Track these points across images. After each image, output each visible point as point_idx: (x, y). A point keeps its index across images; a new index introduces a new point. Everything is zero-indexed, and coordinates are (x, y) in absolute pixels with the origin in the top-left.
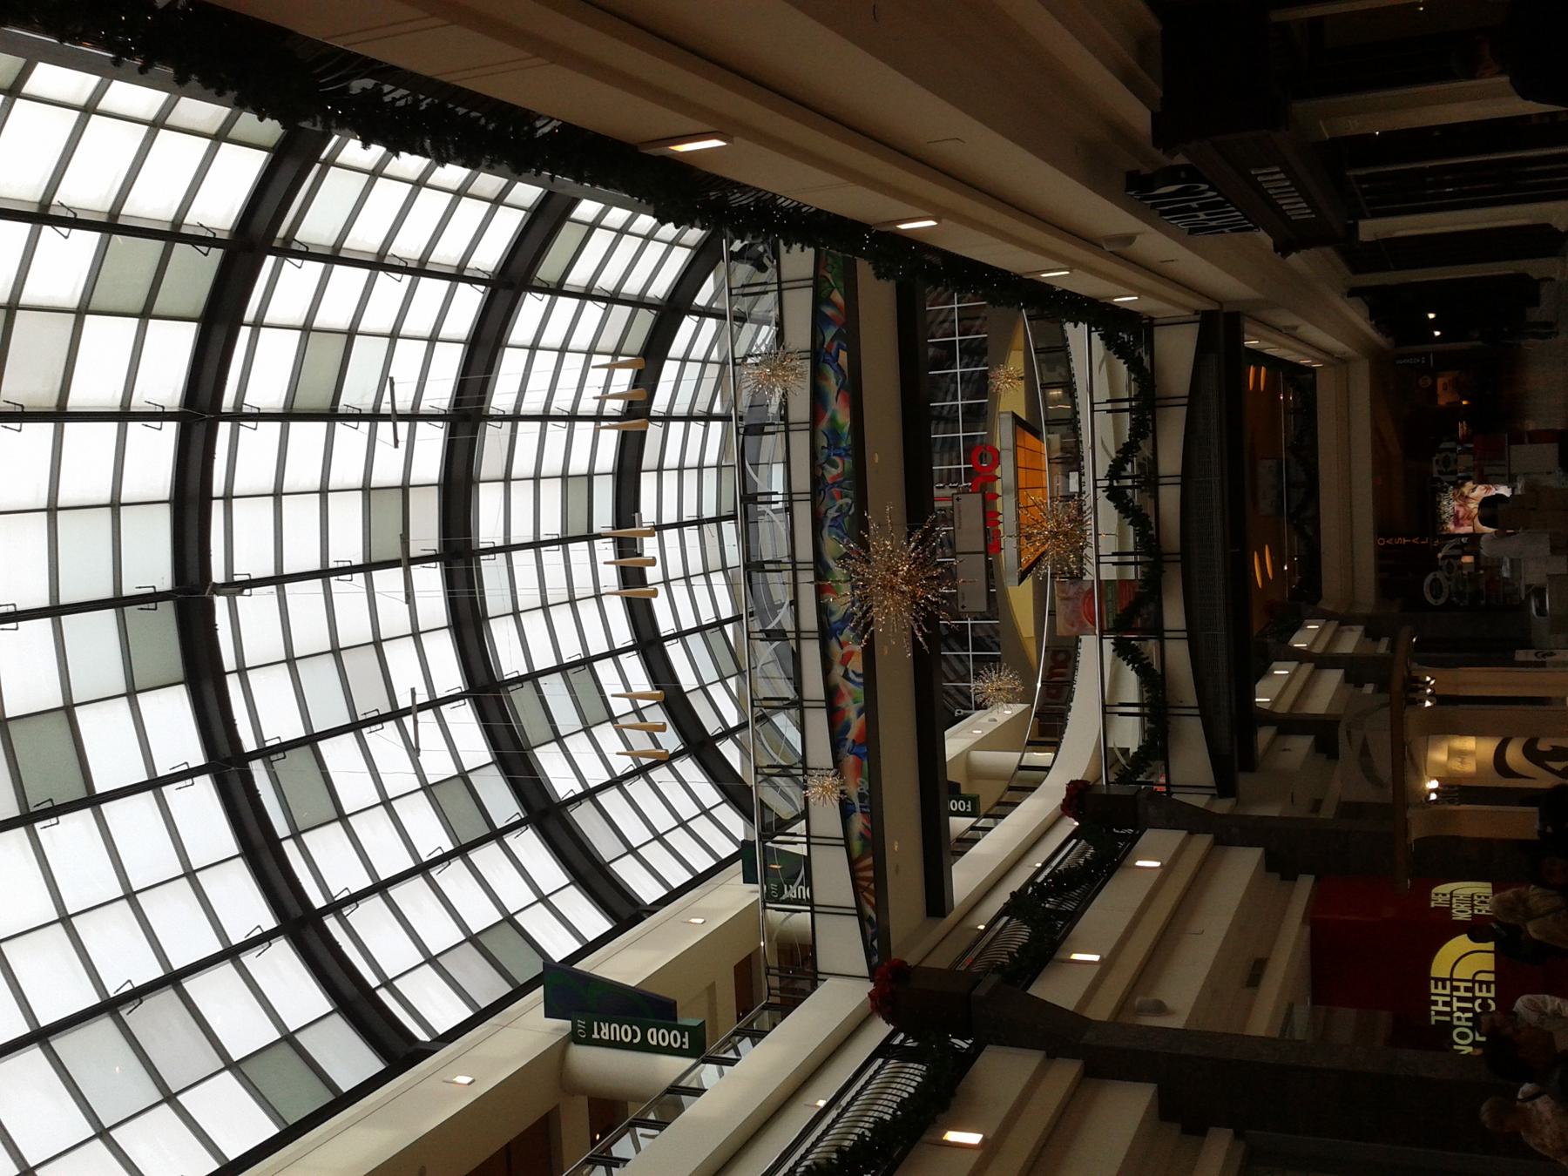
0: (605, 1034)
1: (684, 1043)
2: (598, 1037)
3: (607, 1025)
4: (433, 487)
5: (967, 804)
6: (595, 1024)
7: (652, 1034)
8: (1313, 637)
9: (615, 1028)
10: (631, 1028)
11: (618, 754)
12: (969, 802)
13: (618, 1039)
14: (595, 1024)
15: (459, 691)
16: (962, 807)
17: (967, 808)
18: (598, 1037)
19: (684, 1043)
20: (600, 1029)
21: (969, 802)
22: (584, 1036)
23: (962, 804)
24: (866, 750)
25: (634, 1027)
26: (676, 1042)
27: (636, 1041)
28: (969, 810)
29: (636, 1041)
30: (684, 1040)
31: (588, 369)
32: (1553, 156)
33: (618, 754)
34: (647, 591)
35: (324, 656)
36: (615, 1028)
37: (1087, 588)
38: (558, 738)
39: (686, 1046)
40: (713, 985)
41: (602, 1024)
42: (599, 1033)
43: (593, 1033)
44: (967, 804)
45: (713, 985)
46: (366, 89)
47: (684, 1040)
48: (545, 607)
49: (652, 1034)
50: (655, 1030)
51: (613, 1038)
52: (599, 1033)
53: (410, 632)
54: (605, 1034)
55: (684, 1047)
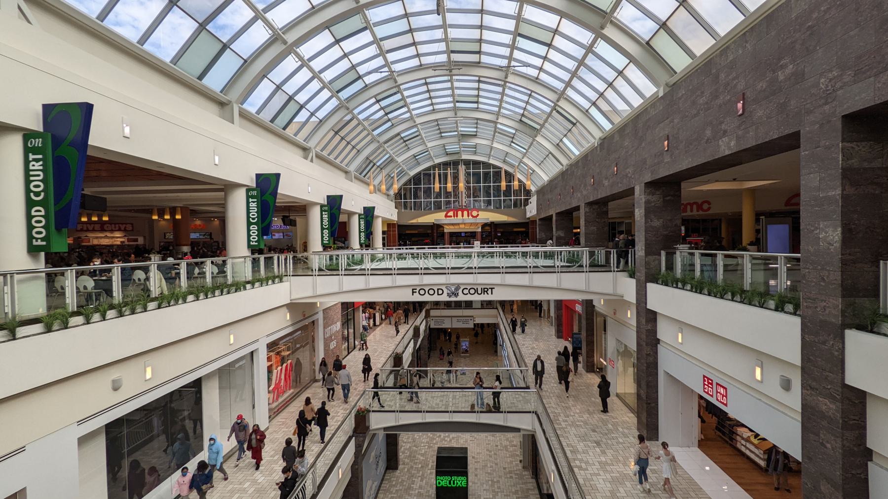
0: (33, 165)
1: (37, 241)
2: (30, 159)
3: (41, 168)
4: (333, 38)
5: (256, 242)
7: (40, 211)
8: (300, 126)
9: (39, 175)
10: (42, 191)
11: (22, 449)
12: (257, 244)
16: (253, 238)
17: (253, 242)
18: (30, 159)
19: (37, 241)
22: (29, 145)
25: (43, 194)
27: (32, 194)
29: (32, 194)
30: (39, 240)
31: (142, 50)
32: (447, 471)
33: (22, 449)
34: (282, 37)
35: (280, 309)
36: (39, 175)
38: (337, 42)
39: (251, 243)
41: (41, 163)
42: (252, 202)
43: (33, 154)
44: (256, 242)
47: (39, 240)
48: (620, 73)
49: (40, 211)
52: (252, 202)
54: (33, 165)
55: (34, 240)
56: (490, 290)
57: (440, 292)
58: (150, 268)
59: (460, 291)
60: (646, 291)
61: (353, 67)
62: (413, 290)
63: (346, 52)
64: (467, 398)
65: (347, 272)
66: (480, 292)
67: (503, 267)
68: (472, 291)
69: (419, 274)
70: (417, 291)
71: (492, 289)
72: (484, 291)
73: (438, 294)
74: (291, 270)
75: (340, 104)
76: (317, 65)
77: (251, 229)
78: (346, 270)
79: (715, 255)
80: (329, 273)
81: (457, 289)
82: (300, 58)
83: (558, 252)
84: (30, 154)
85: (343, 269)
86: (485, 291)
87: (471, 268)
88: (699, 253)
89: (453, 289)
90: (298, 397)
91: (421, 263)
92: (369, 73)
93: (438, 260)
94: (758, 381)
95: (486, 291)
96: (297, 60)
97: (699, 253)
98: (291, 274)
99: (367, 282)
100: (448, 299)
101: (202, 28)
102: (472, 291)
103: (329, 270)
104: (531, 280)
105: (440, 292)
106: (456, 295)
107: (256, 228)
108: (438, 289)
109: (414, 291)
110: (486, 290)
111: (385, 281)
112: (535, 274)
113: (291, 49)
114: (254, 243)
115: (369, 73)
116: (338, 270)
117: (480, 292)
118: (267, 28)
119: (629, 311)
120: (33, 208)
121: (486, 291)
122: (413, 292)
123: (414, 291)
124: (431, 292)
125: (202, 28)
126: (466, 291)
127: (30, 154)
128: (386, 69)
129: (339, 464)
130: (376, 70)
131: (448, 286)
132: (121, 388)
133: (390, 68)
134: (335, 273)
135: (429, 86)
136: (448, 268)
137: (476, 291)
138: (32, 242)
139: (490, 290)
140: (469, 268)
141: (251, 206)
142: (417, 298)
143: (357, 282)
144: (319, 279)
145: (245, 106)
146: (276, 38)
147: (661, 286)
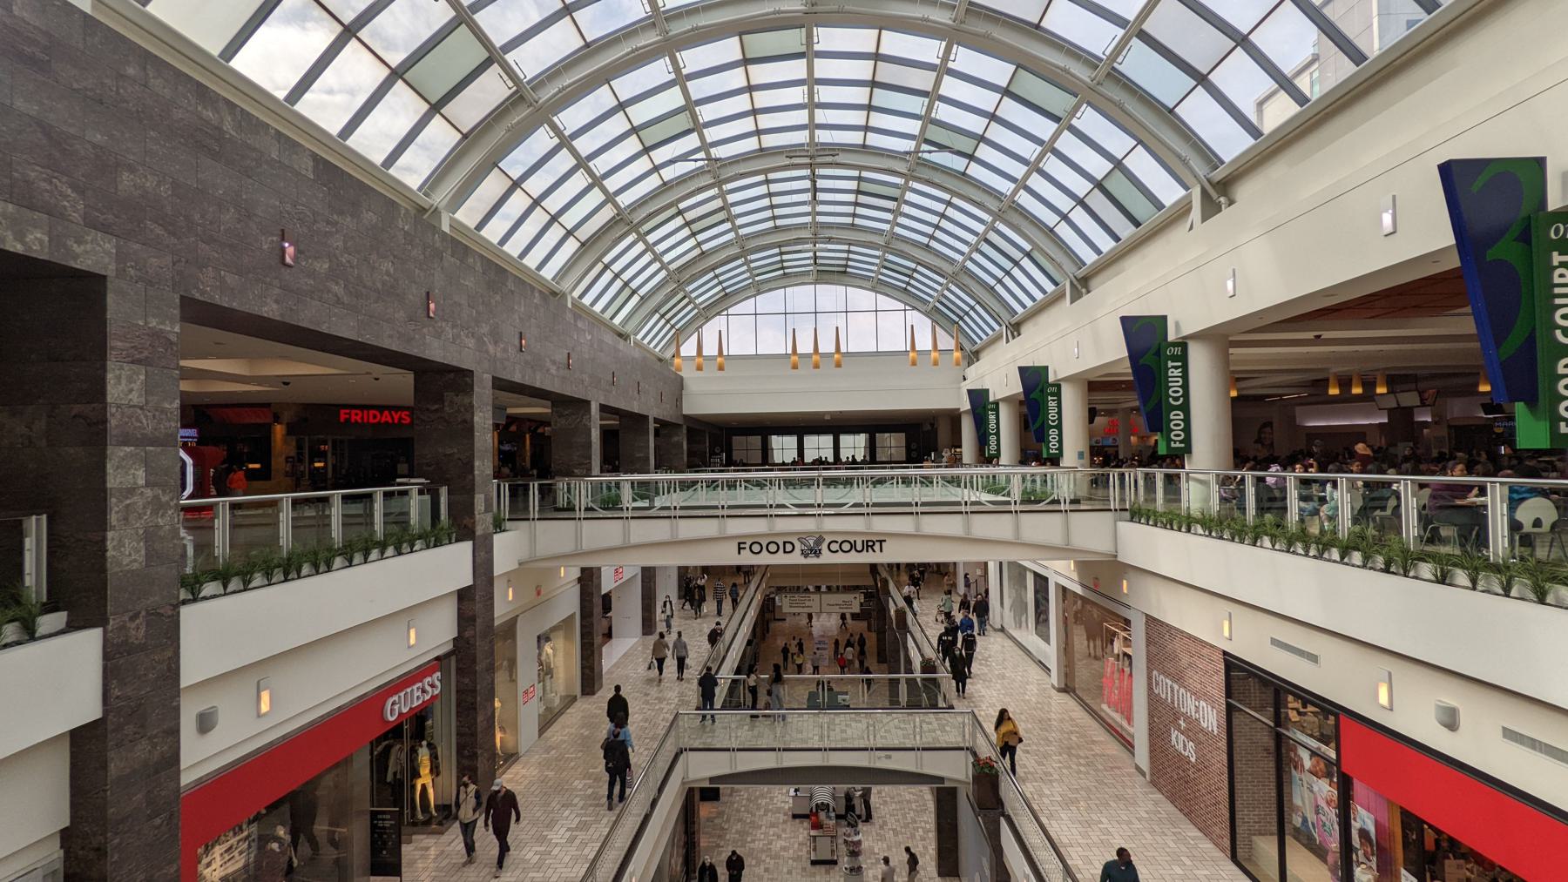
2: (1556, 263)
5: (1181, 442)
6: (1180, 364)
10: (1557, 267)
12: (1183, 445)
13: (1170, 384)
14: (1180, 364)
15: (522, 77)
17: (1175, 442)
18: (1556, 263)
20: (1176, 368)
21: (1183, 445)
22: (1553, 236)
23: (1179, 435)
24: (1425, 431)
26: (1175, 435)
28: (1173, 445)
37: (1506, 406)
38: (1006, 92)
39: (1173, 445)
40: (1505, 729)
42: (1173, 367)
44: (1181, 442)
45: (1505, 729)
46: (66, 828)
50: (1182, 417)
51: (1170, 379)
52: (1173, 367)
53: (621, 100)
54: (1562, 276)
56: (878, 544)
57: (789, 548)
58: (331, 500)
59: (824, 547)
60: (474, 556)
61: (981, 139)
62: (739, 544)
63: (635, 125)
64: (800, 736)
65: (1074, 507)
66: (859, 548)
67: (675, 508)
68: (846, 547)
69: (912, 513)
70: (747, 546)
71: (881, 542)
72: (868, 546)
73: (785, 552)
74: (537, 508)
75: (618, 215)
76: (585, 145)
77: (1172, 417)
78: (587, 509)
79: (369, 496)
80: (603, 513)
81: (820, 541)
82: (558, 132)
83: (722, 482)
84: (1555, 254)
85: (583, 508)
86: (868, 546)
87: (668, 508)
88: (1253, 476)
89: (811, 542)
90: (1123, 745)
91: (723, 497)
92: (672, 162)
93: (790, 491)
94: (1383, 707)
95: (871, 547)
96: (552, 134)
97: (1253, 476)
98: (537, 517)
99: (626, 533)
100: (803, 561)
101: (1239, 40)
102: (846, 547)
103: (604, 509)
104: (968, 527)
105: (789, 548)
106: (818, 553)
107: (1182, 417)
108: (785, 543)
109: (742, 546)
110: (870, 544)
111: (707, 528)
112: (729, 520)
113: (544, 115)
114: (1178, 445)
115: (672, 162)
116: (573, 509)
117: (859, 548)
118: (505, 77)
119: (1125, 582)
120: (1562, 358)
121: (871, 547)
122: (740, 549)
123: (742, 546)
124: (773, 548)
125: (1239, 40)
126: (834, 547)
127: (1555, 254)
128: (702, 155)
129: (630, 868)
130: (684, 157)
131: (802, 537)
132: (212, 732)
133: (708, 153)
134: (566, 515)
135: (771, 185)
136: (868, 505)
137: (853, 546)
138: (1558, 427)
139: (878, 544)
140: (855, 505)
141: (1170, 374)
142: (747, 559)
143: (658, 530)
144: (1075, 518)
145: (459, 215)
146: (517, 99)
147: (450, 547)
